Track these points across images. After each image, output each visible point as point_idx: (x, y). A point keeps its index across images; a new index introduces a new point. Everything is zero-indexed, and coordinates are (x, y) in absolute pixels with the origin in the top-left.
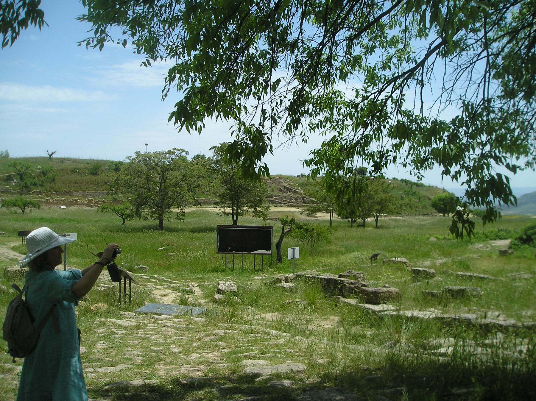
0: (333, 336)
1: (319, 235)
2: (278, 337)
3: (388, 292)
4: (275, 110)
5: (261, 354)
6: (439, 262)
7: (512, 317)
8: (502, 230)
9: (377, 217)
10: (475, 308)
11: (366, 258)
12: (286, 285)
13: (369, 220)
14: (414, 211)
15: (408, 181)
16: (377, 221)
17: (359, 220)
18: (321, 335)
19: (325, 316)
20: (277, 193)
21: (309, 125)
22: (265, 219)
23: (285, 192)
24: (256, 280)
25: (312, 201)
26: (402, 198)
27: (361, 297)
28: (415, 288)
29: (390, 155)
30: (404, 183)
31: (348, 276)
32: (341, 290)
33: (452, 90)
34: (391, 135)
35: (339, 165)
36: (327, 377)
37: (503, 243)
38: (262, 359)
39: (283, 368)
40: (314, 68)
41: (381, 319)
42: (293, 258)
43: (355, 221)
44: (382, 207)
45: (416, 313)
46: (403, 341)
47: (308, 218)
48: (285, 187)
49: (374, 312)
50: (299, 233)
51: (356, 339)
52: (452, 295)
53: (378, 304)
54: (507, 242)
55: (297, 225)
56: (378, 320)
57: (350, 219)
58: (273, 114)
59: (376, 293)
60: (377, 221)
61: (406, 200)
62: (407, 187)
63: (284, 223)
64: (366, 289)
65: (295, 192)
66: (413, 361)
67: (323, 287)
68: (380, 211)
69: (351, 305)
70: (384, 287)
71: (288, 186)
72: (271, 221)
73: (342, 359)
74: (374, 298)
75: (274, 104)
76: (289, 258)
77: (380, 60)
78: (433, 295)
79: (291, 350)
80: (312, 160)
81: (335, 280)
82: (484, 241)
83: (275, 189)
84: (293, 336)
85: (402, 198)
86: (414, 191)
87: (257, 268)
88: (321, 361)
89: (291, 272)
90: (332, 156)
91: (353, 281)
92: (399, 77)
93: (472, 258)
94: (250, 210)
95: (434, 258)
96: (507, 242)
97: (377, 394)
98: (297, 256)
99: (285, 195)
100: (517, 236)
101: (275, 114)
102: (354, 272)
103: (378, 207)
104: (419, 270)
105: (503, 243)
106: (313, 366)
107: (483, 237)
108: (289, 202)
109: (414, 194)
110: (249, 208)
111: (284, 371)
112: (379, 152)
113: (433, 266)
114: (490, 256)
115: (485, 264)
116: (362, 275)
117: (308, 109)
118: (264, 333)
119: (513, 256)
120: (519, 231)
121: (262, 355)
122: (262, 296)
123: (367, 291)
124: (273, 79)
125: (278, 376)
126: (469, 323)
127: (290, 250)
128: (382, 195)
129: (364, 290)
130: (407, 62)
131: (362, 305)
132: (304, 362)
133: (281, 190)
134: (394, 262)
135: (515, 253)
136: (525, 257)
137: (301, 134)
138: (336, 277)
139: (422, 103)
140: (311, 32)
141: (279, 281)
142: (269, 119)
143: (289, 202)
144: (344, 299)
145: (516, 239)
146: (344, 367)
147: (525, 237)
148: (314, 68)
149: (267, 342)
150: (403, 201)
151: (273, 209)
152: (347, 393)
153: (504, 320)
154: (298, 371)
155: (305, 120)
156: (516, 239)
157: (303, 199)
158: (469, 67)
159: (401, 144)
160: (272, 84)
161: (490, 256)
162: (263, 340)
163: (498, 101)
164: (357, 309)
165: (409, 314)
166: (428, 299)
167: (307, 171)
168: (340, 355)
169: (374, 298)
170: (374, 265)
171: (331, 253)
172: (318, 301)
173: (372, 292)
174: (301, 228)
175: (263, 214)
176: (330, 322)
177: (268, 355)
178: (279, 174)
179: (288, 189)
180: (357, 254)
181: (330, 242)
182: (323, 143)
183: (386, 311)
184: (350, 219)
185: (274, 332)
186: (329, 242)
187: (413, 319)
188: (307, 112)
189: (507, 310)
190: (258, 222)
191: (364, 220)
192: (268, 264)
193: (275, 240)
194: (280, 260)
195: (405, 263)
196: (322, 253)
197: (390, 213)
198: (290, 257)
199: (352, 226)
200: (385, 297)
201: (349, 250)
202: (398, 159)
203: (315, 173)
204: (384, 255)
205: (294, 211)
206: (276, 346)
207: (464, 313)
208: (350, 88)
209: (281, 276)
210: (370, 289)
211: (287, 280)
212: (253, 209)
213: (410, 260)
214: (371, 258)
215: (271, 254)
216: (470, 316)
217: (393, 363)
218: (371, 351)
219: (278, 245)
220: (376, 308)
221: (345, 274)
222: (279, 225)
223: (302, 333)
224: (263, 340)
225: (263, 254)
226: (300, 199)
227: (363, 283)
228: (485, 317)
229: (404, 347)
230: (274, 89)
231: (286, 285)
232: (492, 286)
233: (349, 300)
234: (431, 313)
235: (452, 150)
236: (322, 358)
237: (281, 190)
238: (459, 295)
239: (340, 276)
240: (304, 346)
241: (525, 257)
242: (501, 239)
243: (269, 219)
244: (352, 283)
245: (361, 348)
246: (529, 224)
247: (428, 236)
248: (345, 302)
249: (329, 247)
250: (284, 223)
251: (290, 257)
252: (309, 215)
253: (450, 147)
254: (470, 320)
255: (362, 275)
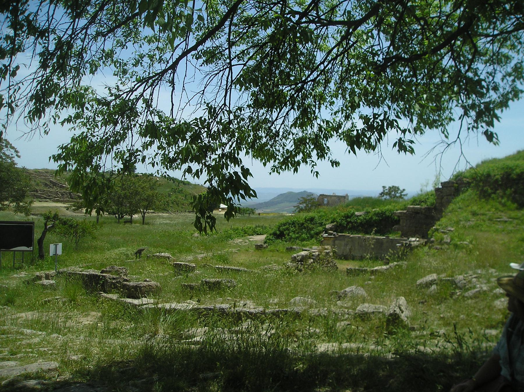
0: (92, 330)
1: (84, 231)
2: (31, 336)
3: (149, 286)
4: (13, 98)
5: (11, 355)
6: (200, 256)
7: (261, 305)
8: (259, 227)
9: (144, 214)
10: (229, 298)
11: (131, 254)
12: (45, 282)
13: (136, 216)
14: (180, 208)
15: (175, 179)
16: (143, 217)
17: (127, 217)
18: (78, 332)
19: (86, 313)
20: (42, 187)
21: (53, 116)
22: (27, 214)
23: (51, 187)
24: (15, 278)
25: (79, 196)
26: (169, 195)
27: (122, 292)
28: (176, 281)
29: (139, 155)
30: (172, 181)
31: (110, 272)
32: (103, 285)
33: (203, 94)
34: (143, 134)
35: (88, 162)
36: (82, 373)
37: (260, 239)
38: (11, 360)
39: (33, 368)
40: (61, 58)
41: (140, 312)
42: (56, 254)
43: (122, 217)
44: (149, 203)
45: (174, 305)
46: (161, 332)
47: (74, 214)
48: (51, 182)
49: (135, 306)
50: (63, 229)
51: (114, 333)
52: (210, 287)
53: (138, 298)
54: (263, 237)
55: (61, 220)
56: (138, 313)
57: (117, 215)
58: (10, 102)
59: (136, 287)
60: (143, 217)
61: (173, 197)
62: (174, 185)
63: (47, 218)
64: (128, 283)
65: (61, 187)
66: (165, 351)
67: (85, 283)
68: (147, 208)
69: (112, 300)
70: (146, 281)
71: (54, 181)
72: (34, 217)
73: (97, 354)
74: (135, 292)
75: (11, 92)
76: (51, 254)
77: (133, 56)
78: (192, 288)
79: (44, 349)
80: (59, 156)
81: (97, 275)
82: (242, 236)
83: (40, 184)
84: (49, 334)
85: (169, 195)
86: (180, 189)
87: (17, 265)
88: (75, 358)
89: (53, 269)
90: (82, 152)
91: (115, 277)
92: (150, 78)
93: (231, 252)
94: (11, 204)
95: (196, 252)
96: (263, 237)
97: (128, 385)
98: (60, 252)
99: (51, 190)
100: (272, 232)
101: (12, 102)
102: (117, 268)
103: (145, 203)
104: (181, 264)
105: (260, 239)
106: (66, 363)
107: (242, 233)
108: (55, 197)
109: (181, 192)
110: (11, 202)
111: (34, 371)
112: (129, 151)
113: (196, 261)
114: (247, 251)
115: (242, 258)
116: (124, 271)
117: (55, 100)
118: (17, 333)
119: (267, 250)
120: (274, 228)
121: (12, 357)
122: (19, 295)
123: (128, 286)
124: (14, 65)
125: (27, 377)
126: (222, 311)
127: (52, 247)
128: (150, 192)
129: (125, 285)
130: (159, 63)
131: (123, 299)
132: (57, 360)
133: (46, 185)
134: (158, 257)
135: (269, 247)
136: (277, 251)
137: (44, 125)
138: (98, 273)
139: (173, 105)
140: (61, 19)
141: (39, 278)
142: (6, 106)
143: (55, 197)
144: (105, 295)
145: (270, 235)
146: (98, 362)
147: (278, 232)
148: (61, 58)
149: (20, 342)
150: (170, 199)
151: (37, 204)
152: (98, 387)
153: (254, 308)
154: (49, 370)
155: (50, 111)
156: (270, 235)
157: (70, 195)
158: (218, 73)
159: (151, 143)
160: (12, 69)
161: (247, 251)
162: (16, 340)
163: (248, 110)
164: (118, 304)
165: (167, 306)
166: (188, 291)
167: (54, 166)
168: (95, 350)
169: (135, 292)
170: (138, 260)
171: (96, 249)
172: (79, 298)
173: (133, 287)
174: (65, 223)
175: (25, 209)
176: (88, 319)
177: (19, 356)
178: (45, 168)
179: (55, 184)
180: (123, 249)
181: (95, 238)
182: (72, 138)
183: (145, 304)
184: (117, 215)
185: (29, 331)
186: (94, 238)
187: (169, 312)
188: (53, 103)
189: (256, 299)
190: (20, 217)
191: (132, 217)
192: (29, 261)
193: (37, 236)
194: (42, 256)
195: (168, 257)
196: (87, 249)
197: (158, 209)
198: (52, 253)
199: (119, 222)
200: (146, 291)
201: (115, 245)
202: (147, 159)
203: (63, 168)
204: (149, 250)
205: (61, 207)
206: (29, 345)
207: (219, 303)
208: (101, 83)
209: (42, 273)
210: (131, 284)
211: (47, 277)
212: (15, 204)
213: (173, 254)
214: (136, 253)
215: (32, 251)
216: (224, 306)
217: (147, 354)
218: (128, 344)
219: (40, 241)
220: (136, 302)
221: (108, 270)
222: (42, 219)
223: (58, 331)
224: (16, 340)
225: (23, 251)
226: (66, 194)
227: (125, 278)
228: (235, 306)
229: (161, 338)
230: (14, 74)
231: (45, 282)
232: (245, 277)
233: (110, 296)
234: (191, 304)
235: (194, 150)
236: (77, 355)
237: (46, 185)
238: (215, 287)
239: (103, 272)
240: (58, 344)
241: (277, 251)
242: (258, 234)
243: (33, 215)
244: (114, 279)
245: (118, 342)
246: (283, 221)
247: (193, 232)
248: (107, 298)
249: (95, 243)
250: (47, 218)
251: (52, 253)
252: (74, 210)
253: (192, 147)
254: (223, 309)
255: (124, 271)
